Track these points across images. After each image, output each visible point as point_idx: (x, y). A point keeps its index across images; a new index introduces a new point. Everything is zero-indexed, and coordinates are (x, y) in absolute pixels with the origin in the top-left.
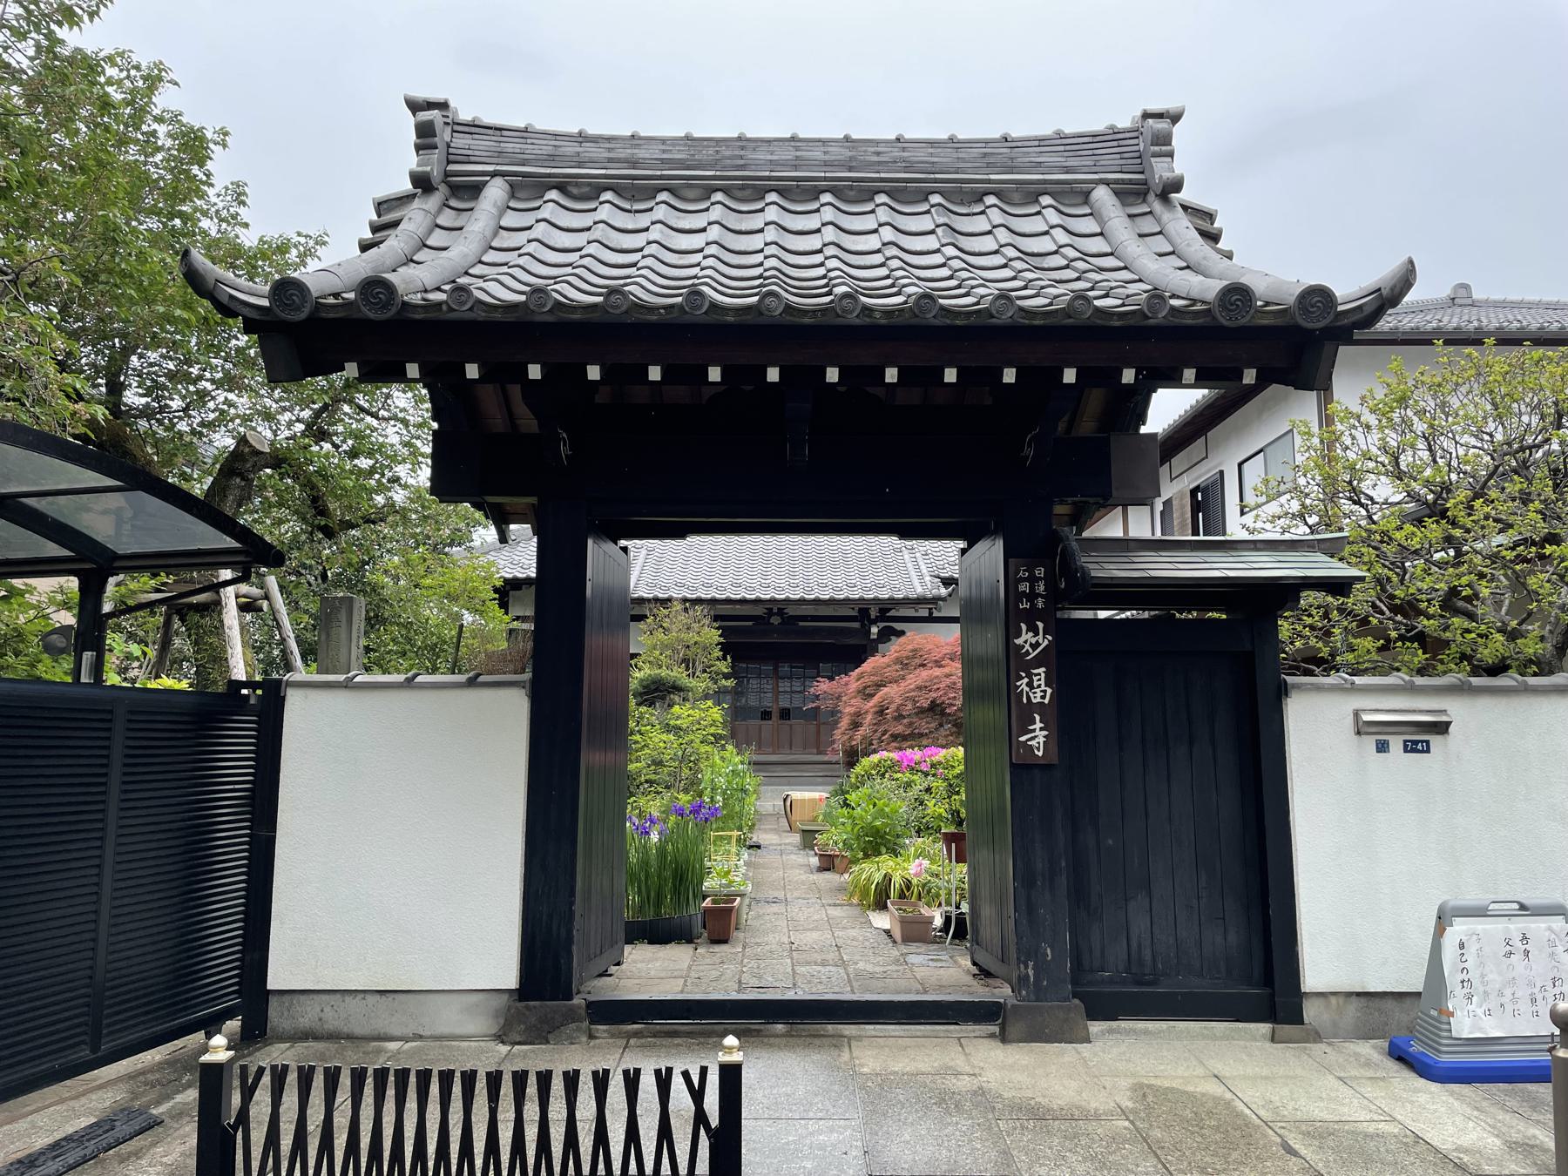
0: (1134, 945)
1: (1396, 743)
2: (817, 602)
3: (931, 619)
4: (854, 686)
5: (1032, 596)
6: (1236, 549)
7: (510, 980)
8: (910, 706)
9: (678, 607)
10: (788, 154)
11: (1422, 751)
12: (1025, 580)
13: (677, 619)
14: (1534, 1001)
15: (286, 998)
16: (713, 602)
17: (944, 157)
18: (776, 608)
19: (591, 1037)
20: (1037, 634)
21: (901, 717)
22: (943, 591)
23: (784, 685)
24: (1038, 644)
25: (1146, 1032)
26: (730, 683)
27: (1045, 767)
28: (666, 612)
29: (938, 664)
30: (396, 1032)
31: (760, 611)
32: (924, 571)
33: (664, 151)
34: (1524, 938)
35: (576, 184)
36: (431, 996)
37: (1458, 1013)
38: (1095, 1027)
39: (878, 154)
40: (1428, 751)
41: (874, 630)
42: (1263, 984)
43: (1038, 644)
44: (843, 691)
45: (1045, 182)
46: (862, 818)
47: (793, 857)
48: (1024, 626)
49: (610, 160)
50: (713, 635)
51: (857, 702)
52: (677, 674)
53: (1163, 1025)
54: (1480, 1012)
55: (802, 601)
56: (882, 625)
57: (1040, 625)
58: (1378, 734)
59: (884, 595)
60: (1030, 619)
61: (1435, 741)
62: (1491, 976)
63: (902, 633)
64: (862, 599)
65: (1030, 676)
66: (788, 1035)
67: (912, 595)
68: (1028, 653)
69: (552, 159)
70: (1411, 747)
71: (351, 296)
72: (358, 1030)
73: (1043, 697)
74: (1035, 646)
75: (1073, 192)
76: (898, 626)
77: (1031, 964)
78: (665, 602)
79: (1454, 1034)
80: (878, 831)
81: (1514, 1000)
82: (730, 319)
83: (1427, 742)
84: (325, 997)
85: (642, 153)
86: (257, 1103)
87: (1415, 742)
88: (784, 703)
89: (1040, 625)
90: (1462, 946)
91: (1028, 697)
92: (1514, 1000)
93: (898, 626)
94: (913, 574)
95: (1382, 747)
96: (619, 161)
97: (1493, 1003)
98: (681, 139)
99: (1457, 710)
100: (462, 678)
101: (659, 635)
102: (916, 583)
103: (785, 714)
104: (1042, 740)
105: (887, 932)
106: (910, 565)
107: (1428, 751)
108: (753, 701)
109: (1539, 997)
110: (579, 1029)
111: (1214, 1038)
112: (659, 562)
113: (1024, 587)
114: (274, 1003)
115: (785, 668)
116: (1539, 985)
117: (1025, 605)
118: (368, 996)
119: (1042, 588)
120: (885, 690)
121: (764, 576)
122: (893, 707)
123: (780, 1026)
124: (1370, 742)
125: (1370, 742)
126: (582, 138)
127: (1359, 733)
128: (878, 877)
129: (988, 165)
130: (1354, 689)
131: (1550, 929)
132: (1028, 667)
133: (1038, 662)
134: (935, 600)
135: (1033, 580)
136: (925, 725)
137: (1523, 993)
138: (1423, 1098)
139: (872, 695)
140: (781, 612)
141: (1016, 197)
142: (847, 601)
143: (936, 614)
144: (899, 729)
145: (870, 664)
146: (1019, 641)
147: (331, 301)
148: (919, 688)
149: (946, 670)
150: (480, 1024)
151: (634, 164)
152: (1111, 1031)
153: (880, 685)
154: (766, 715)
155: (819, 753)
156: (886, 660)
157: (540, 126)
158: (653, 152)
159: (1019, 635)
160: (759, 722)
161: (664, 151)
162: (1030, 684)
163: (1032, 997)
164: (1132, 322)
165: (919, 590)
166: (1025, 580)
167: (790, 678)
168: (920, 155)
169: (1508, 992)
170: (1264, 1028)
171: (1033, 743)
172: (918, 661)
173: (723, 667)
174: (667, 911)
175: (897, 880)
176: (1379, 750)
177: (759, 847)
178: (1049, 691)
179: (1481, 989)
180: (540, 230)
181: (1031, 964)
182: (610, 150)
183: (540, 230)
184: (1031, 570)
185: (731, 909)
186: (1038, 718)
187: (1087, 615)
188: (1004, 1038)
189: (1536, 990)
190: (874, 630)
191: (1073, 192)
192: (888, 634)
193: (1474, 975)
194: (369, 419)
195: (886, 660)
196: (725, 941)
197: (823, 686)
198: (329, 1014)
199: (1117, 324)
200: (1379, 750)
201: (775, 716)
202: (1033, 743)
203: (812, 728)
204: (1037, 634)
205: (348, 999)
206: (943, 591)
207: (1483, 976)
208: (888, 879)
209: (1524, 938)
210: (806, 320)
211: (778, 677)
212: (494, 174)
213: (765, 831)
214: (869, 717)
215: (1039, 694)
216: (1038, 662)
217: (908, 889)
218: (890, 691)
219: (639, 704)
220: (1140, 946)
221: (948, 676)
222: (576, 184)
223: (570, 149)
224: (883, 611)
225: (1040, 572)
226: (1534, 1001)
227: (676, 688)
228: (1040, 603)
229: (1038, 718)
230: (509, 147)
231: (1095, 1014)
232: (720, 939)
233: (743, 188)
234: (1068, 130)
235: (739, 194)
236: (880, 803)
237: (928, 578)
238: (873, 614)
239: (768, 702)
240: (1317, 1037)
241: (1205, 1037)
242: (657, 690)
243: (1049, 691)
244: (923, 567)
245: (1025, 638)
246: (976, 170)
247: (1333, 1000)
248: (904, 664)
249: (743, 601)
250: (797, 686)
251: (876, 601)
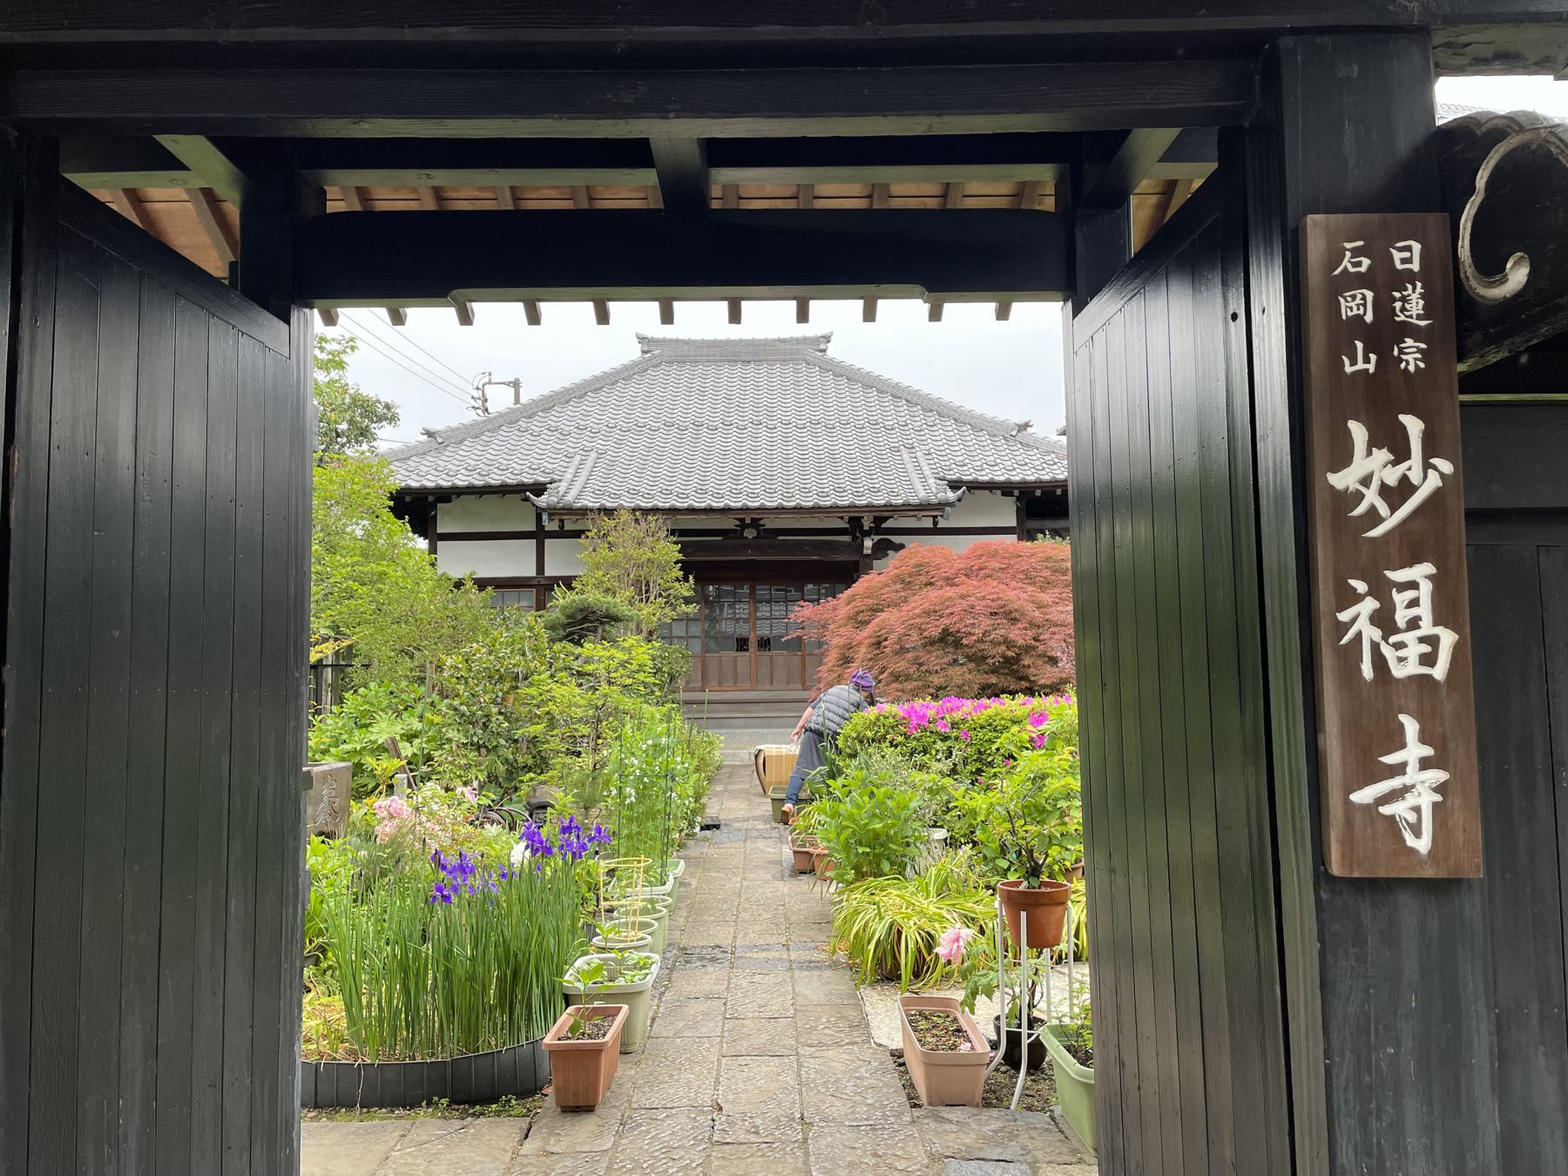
2: (798, 510)
3: (936, 531)
4: (844, 611)
5: (1383, 334)
8: (915, 637)
9: (625, 517)
12: (1362, 281)
13: (627, 533)
16: (673, 511)
18: (750, 519)
20: (1401, 453)
21: (903, 650)
22: (951, 496)
23: (764, 610)
24: (1405, 488)
26: (692, 609)
27: (1438, 889)
28: (612, 523)
29: (950, 581)
31: (730, 523)
32: (928, 473)
41: (868, 543)
44: (825, 616)
46: (851, 817)
47: (761, 844)
48: (1358, 432)
50: (670, 551)
51: (848, 631)
52: (619, 602)
55: (780, 510)
56: (877, 538)
57: (1414, 426)
59: (880, 500)
60: (1381, 403)
63: (902, 546)
64: (852, 506)
65: (1381, 589)
67: (914, 501)
68: (1373, 517)
73: (1429, 660)
74: (1397, 494)
76: (896, 539)
78: (609, 512)
80: (877, 835)
88: (764, 630)
89: (1360, 345)
91: (1380, 662)
93: (896, 539)
94: (915, 477)
101: (604, 551)
102: (918, 486)
103: (764, 644)
104: (1426, 799)
105: (897, 1055)
106: (909, 466)
108: (726, 627)
112: (611, 465)
113: (1358, 305)
115: (763, 591)
117: (1362, 363)
119: (1416, 305)
120: (883, 616)
121: (736, 479)
122: (893, 637)
128: (880, 930)
132: (1375, 565)
133: (1408, 545)
134: (942, 506)
135: (1386, 282)
136: (935, 659)
139: (867, 623)
140: (755, 523)
142: (834, 509)
143: (942, 524)
144: (901, 665)
145: (862, 584)
146: (1342, 480)
148: (927, 613)
149: (962, 590)
153: (875, 610)
154: (742, 644)
155: (805, 689)
156: (882, 578)
159: (1343, 459)
160: (733, 654)
162: (1384, 620)
165: (922, 494)
166: (1362, 281)
167: (768, 602)
172: (923, 579)
173: (686, 590)
174: (492, 1042)
175: (911, 936)
177: (717, 827)
178: (1448, 638)
184: (1377, 249)
185: (596, 1052)
186: (1411, 726)
190: (868, 543)
192: (882, 549)
194: (1358, 830)
195: (882, 578)
196: (589, 1109)
197: (804, 611)
201: (753, 644)
203: (796, 660)
206: (951, 496)
208: (896, 933)
211: (755, 600)
213: (734, 795)
214: (863, 650)
215: (1415, 650)
216: (1408, 545)
217: (930, 948)
218: (888, 617)
219: (552, 641)
221: (963, 597)
224: (879, 520)
225: (1408, 255)
227: (613, 619)
228: (1411, 355)
229: (1411, 726)
232: (579, 1106)
236: (880, 793)
237: (932, 481)
238: (867, 524)
239: (743, 630)
242: (585, 620)
243: (1448, 638)
244: (926, 467)
245: (1364, 469)
248: (906, 582)
249: (709, 511)
250: (778, 610)
251: (870, 508)
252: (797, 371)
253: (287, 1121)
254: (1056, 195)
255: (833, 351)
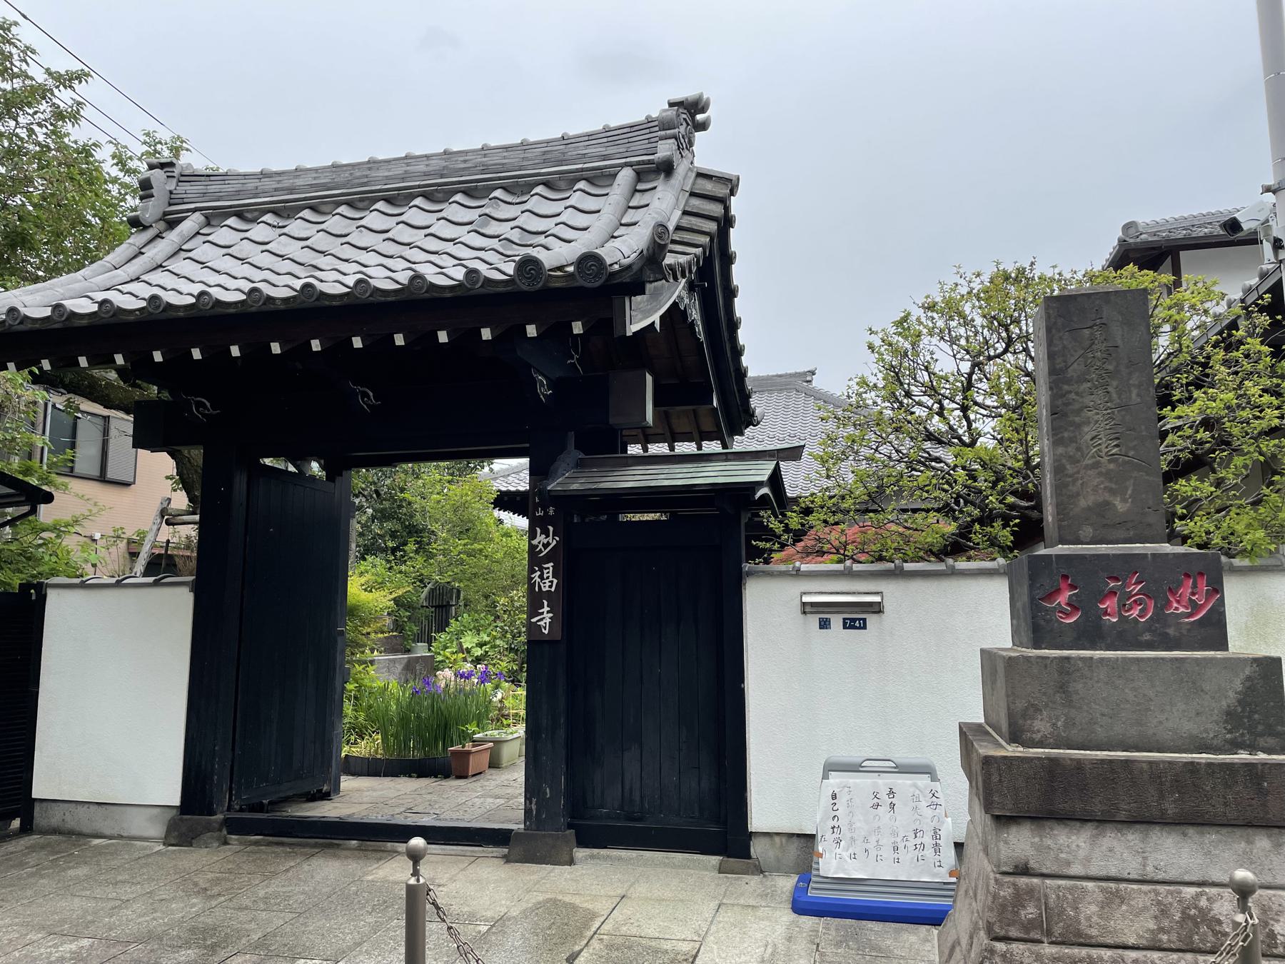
0: (627, 787)
1: (836, 621)
6: (711, 461)
7: (176, 800)
10: (399, 170)
11: (860, 628)
14: (896, 849)
15: (45, 804)
17: (513, 158)
19: (226, 843)
20: (548, 536)
24: (548, 544)
25: (620, 859)
30: (107, 832)
33: (315, 178)
34: (891, 792)
35: (248, 211)
36: (128, 808)
37: (827, 855)
38: (580, 853)
39: (465, 161)
40: (864, 627)
42: (714, 822)
43: (548, 544)
45: (582, 170)
48: (539, 530)
49: (276, 190)
53: (633, 854)
54: (846, 855)
57: (551, 528)
58: (821, 613)
61: (872, 620)
62: (858, 824)
65: (541, 570)
66: (359, 849)
68: (541, 551)
69: (238, 194)
70: (849, 624)
71: (571, 269)
72: (86, 830)
74: (546, 546)
75: (603, 176)
77: (534, 800)
79: (822, 873)
81: (878, 846)
82: (181, 314)
83: (864, 620)
84: (66, 805)
85: (299, 182)
86: (928, 931)
87: (854, 620)
89: (551, 528)
90: (834, 796)
92: (878, 846)
95: (824, 624)
96: (282, 189)
97: (858, 849)
98: (328, 167)
99: (893, 594)
100: (151, 580)
107: (864, 627)
109: (901, 846)
110: (212, 838)
111: (674, 866)
114: (37, 808)
116: (901, 835)
118: (92, 807)
123: (354, 842)
124: (814, 620)
125: (814, 620)
126: (264, 175)
127: (804, 613)
129: (545, 161)
130: (797, 574)
131: (915, 786)
133: (548, 558)
137: (887, 841)
138: (905, 936)
141: (562, 185)
147: (559, 273)
150: (157, 830)
151: (291, 190)
152: (592, 857)
157: (418, 152)
158: (308, 180)
161: (315, 178)
162: (541, 577)
163: (534, 827)
164: (459, 293)
168: (495, 159)
169: (873, 839)
170: (715, 860)
171: (542, 623)
176: (821, 627)
178: (555, 581)
179: (849, 835)
180: (568, 216)
181: (534, 800)
182: (279, 182)
183: (568, 216)
187: (638, 517)
188: (507, 859)
189: (899, 840)
191: (603, 176)
193: (843, 823)
198: (68, 817)
199: (449, 295)
200: (821, 627)
202: (542, 623)
204: (548, 536)
205: (79, 807)
207: (851, 824)
209: (891, 792)
210: (232, 311)
212: (623, 166)
216: (548, 558)
220: (631, 789)
222: (248, 211)
223: (251, 184)
226: (896, 849)
230: (212, 188)
231: (583, 842)
233: (361, 200)
234: (613, 124)
235: (360, 205)
240: (759, 870)
241: (666, 865)
243: (555, 581)
246: (535, 166)
247: (777, 839)
252: (788, 397)
253: (994, 682)
254: (134, 436)
255: (817, 382)
